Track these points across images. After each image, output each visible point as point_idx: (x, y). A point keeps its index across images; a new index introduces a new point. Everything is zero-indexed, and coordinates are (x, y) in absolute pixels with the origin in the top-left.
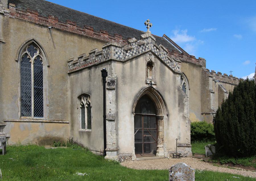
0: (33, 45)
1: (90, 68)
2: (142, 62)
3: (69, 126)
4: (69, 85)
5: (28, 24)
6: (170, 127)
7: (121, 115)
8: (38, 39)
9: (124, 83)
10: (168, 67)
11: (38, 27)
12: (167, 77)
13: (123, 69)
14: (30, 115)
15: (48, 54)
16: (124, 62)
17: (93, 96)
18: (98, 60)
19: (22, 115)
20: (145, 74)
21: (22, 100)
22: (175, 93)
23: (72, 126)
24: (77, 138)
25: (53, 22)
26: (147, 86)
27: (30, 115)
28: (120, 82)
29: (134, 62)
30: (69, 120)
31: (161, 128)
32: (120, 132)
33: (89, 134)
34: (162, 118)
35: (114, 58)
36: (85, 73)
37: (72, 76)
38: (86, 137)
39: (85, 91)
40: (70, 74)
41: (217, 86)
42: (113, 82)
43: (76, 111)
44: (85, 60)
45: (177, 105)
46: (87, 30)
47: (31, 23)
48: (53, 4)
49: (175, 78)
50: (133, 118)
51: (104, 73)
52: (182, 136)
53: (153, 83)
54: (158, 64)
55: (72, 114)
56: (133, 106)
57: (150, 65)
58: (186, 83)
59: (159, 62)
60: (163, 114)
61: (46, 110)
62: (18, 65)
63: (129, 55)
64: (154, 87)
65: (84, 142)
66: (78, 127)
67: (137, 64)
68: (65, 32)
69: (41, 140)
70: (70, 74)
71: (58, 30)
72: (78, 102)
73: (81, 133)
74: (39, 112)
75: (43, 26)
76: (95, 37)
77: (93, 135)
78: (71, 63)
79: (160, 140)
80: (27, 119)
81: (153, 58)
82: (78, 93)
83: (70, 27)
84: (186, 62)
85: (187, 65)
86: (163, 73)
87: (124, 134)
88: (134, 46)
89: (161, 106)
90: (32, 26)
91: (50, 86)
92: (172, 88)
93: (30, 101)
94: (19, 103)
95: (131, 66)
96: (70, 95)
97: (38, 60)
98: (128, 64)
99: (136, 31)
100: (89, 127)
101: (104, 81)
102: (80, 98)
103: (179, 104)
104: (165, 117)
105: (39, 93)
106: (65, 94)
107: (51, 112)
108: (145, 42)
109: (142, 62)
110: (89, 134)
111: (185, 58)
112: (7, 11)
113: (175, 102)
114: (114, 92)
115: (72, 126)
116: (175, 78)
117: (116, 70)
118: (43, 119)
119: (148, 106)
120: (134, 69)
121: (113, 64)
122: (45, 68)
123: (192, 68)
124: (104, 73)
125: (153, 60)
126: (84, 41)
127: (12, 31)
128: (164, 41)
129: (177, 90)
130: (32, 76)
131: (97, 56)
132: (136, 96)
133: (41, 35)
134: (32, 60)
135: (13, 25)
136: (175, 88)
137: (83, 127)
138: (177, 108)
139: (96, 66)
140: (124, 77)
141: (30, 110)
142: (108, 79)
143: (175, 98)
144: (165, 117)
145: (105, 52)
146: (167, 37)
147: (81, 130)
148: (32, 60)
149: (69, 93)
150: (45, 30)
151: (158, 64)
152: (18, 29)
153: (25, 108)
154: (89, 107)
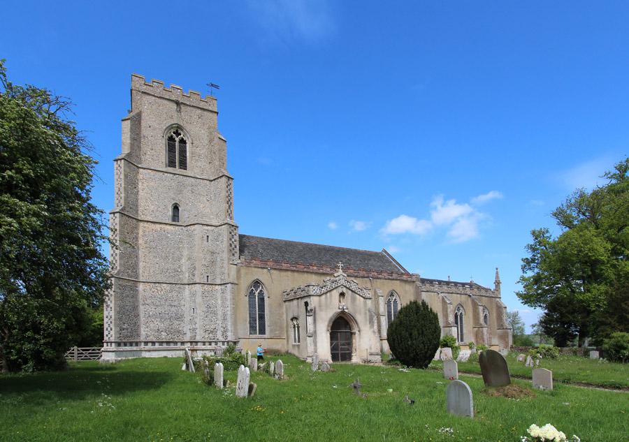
0: (257, 283)
1: (298, 299)
2: (336, 294)
3: (285, 341)
4: (284, 310)
5: (253, 269)
6: (362, 340)
7: (318, 332)
8: (261, 279)
9: (321, 310)
10: (360, 295)
11: (260, 270)
12: (358, 302)
13: (320, 301)
14: (256, 334)
15: (268, 288)
16: (320, 296)
17: (300, 319)
18: (303, 294)
19: (251, 334)
20: (338, 301)
21: (250, 323)
22: (366, 314)
23: (288, 341)
24: (291, 350)
25: (271, 264)
26: (340, 310)
27: (256, 334)
28: (317, 309)
29: (328, 294)
30: (285, 337)
31: (354, 341)
32: (318, 345)
33: (298, 346)
34: (355, 333)
35: (313, 294)
36: (295, 302)
37: (287, 303)
38: (297, 348)
39: (296, 315)
40: (285, 301)
41: (441, 298)
42: (311, 310)
43: (290, 329)
44: (295, 293)
45: (368, 322)
46: (298, 266)
47: (255, 267)
48: (272, 240)
49: (365, 303)
50: (329, 335)
51: (306, 304)
52: (373, 347)
53: (345, 308)
54: (349, 294)
55: (287, 331)
56: (328, 326)
57: (342, 294)
58: (398, 299)
59: (350, 292)
60: (355, 330)
61: (267, 329)
62: (247, 298)
63: (324, 290)
64: (346, 311)
65: (296, 352)
66: (292, 342)
67: (331, 296)
68: (281, 270)
69: (94, 254)
70: (285, 301)
71: (275, 269)
72: (291, 323)
73: (294, 346)
74: (262, 331)
75: (264, 268)
76: (305, 270)
77: (301, 347)
78: (285, 294)
79: (354, 350)
80: (254, 336)
81: (344, 290)
82: (291, 316)
83: (285, 266)
84: (397, 280)
85: (398, 282)
86: (354, 300)
87: (322, 347)
88: (329, 283)
89: (355, 326)
90: (256, 269)
91: (270, 311)
92: (363, 310)
93: (256, 324)
94: (248, 325)
95: (326, 297)
96: (286, 318)
97: (261, 293)
98: (324, 296)
99: (351, 250)
100: (299, 341)
101: (307, 309)
102: (292, 320)
103: (370, 322)
104: (357, 332)
105: (262, 317)
106: (281, 317)
107: (271, 331)
108: (337, 279)
109: (336, 294)
110: (298, 346)
111: (395, 276)
112: (239, 261)
113: (366, 320)
114: (312, 317)
115: (288, 341)
116: (365, 303)
117: (313, 302)
118: (265, 336)
119: (342, 326)
120: (329, 300)
121: (312, 298)
122: (266, 298)
123: (403, 284)
124: (306, 304)
125: (344, 292)
126: (296, 274)
127: (242, 276)
128: (383, 256)
129: (367, 312)
130: (257, 304)
131: (302, 291)
132: (331, 319)
133: (263, 275)
134: (257, 294)
135: (243, 271)
136: (366, 310)
137: (295, 342)
138: (369, 326)
139: (301, 298)
140: (320, 306)
141: (256, 330)
142: (309, 308)
143: (366, 317)
144: (357, 332)
145: (306, 289)
146: (386, 252)
147: (294, 343)
148: (257, 294)
149: (285, 316)
150: (265, 270)
151: (349, 294)
152: (246, 274)
153: (252, 328)
154: (298, 327)
